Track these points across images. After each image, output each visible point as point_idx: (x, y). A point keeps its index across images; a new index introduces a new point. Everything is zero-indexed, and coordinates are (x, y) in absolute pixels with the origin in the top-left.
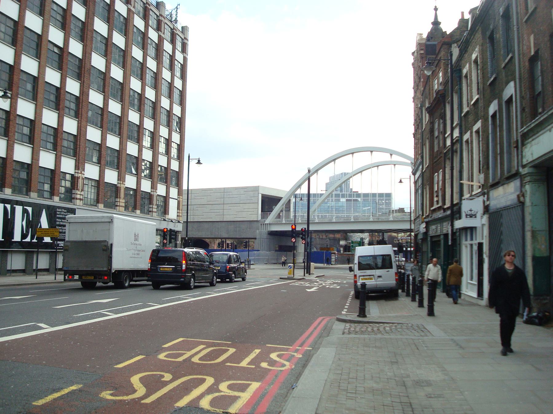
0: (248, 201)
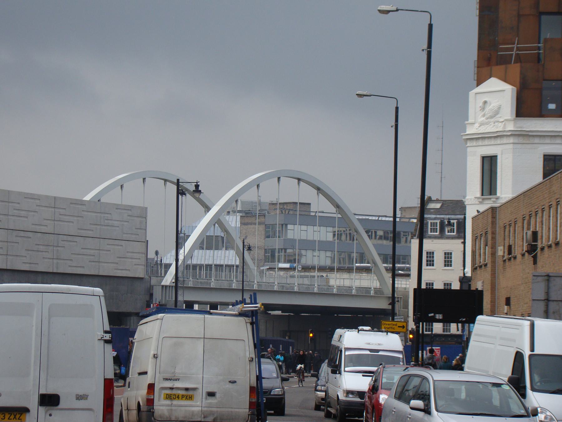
0: (133, 237)
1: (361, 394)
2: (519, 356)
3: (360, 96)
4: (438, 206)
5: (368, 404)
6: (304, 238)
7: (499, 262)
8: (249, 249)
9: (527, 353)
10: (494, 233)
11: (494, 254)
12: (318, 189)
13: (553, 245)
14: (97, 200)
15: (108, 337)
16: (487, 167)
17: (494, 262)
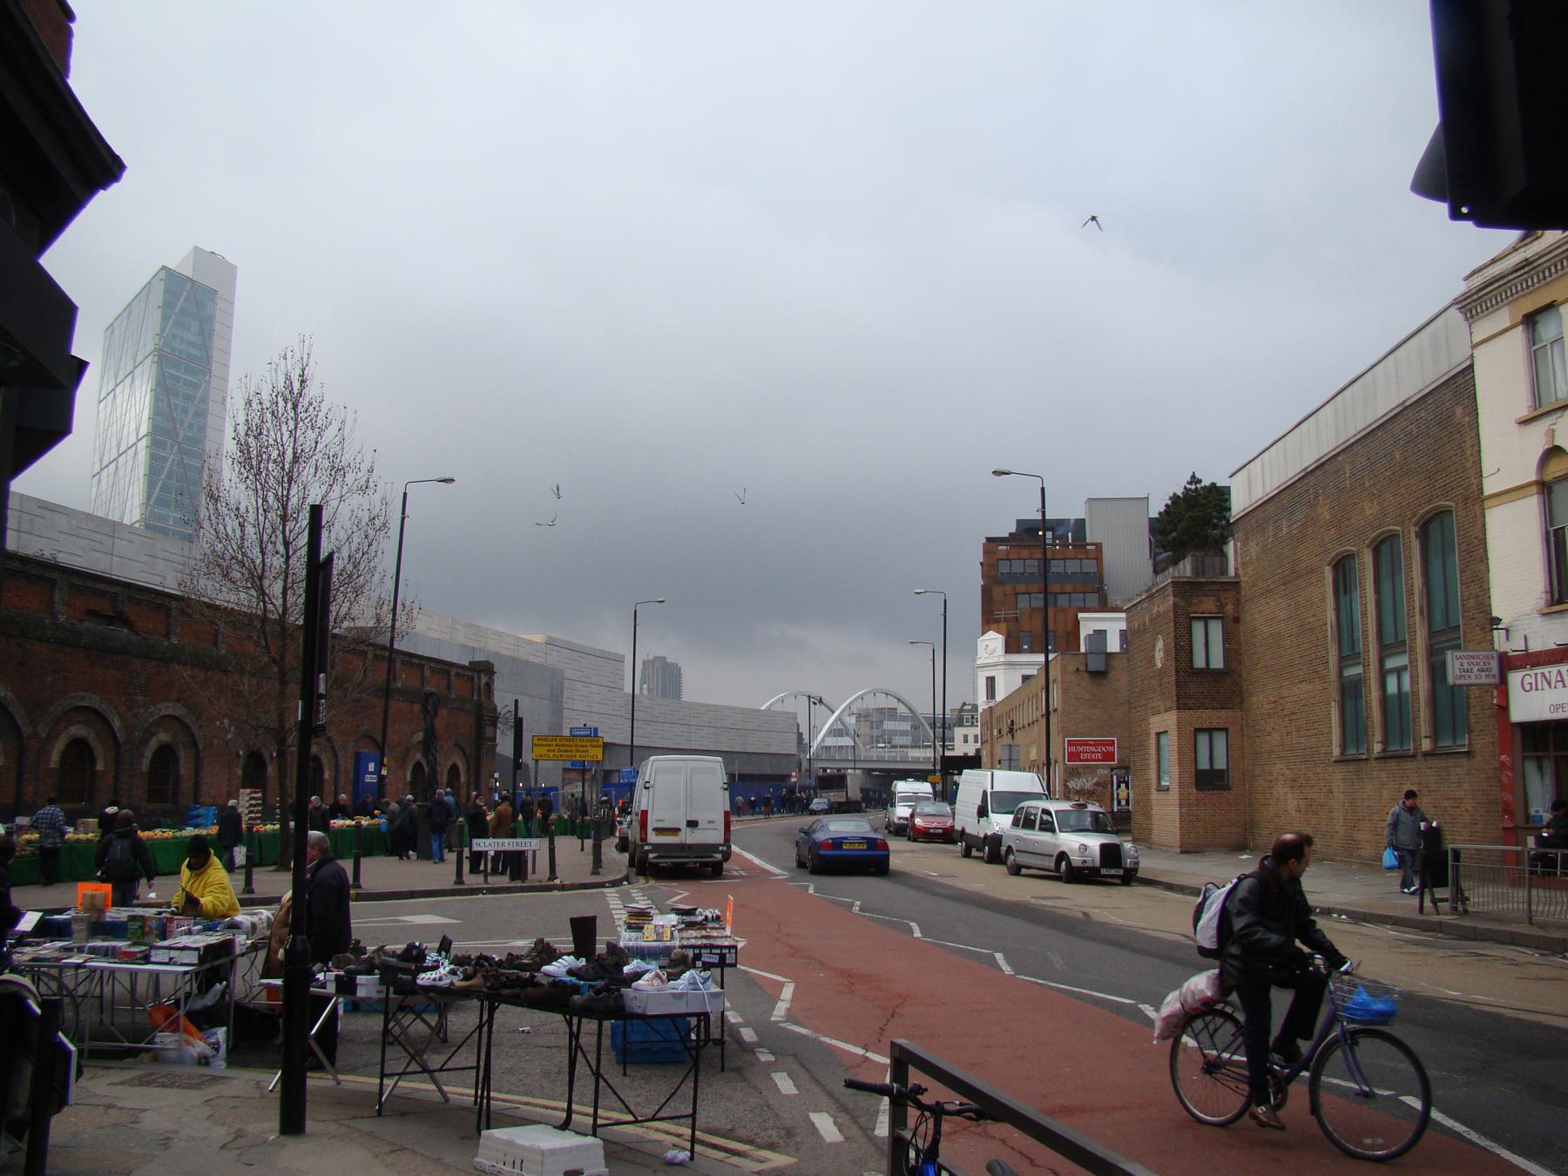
1: (906, 819)
2: (985, 793)
3: (912, 643)
4: (970, 707)
5: (910, 825)
6: (901, 729)
7: (995, 738)
8: (858, 736)
9: (989, 791)
10: (991, 722)
11: (992, 734)
12: (898, 699)
13: (1027, 726)
14: (769, 709)
15: (725, 786)
16: (989, 683)
17: (992, 739)
